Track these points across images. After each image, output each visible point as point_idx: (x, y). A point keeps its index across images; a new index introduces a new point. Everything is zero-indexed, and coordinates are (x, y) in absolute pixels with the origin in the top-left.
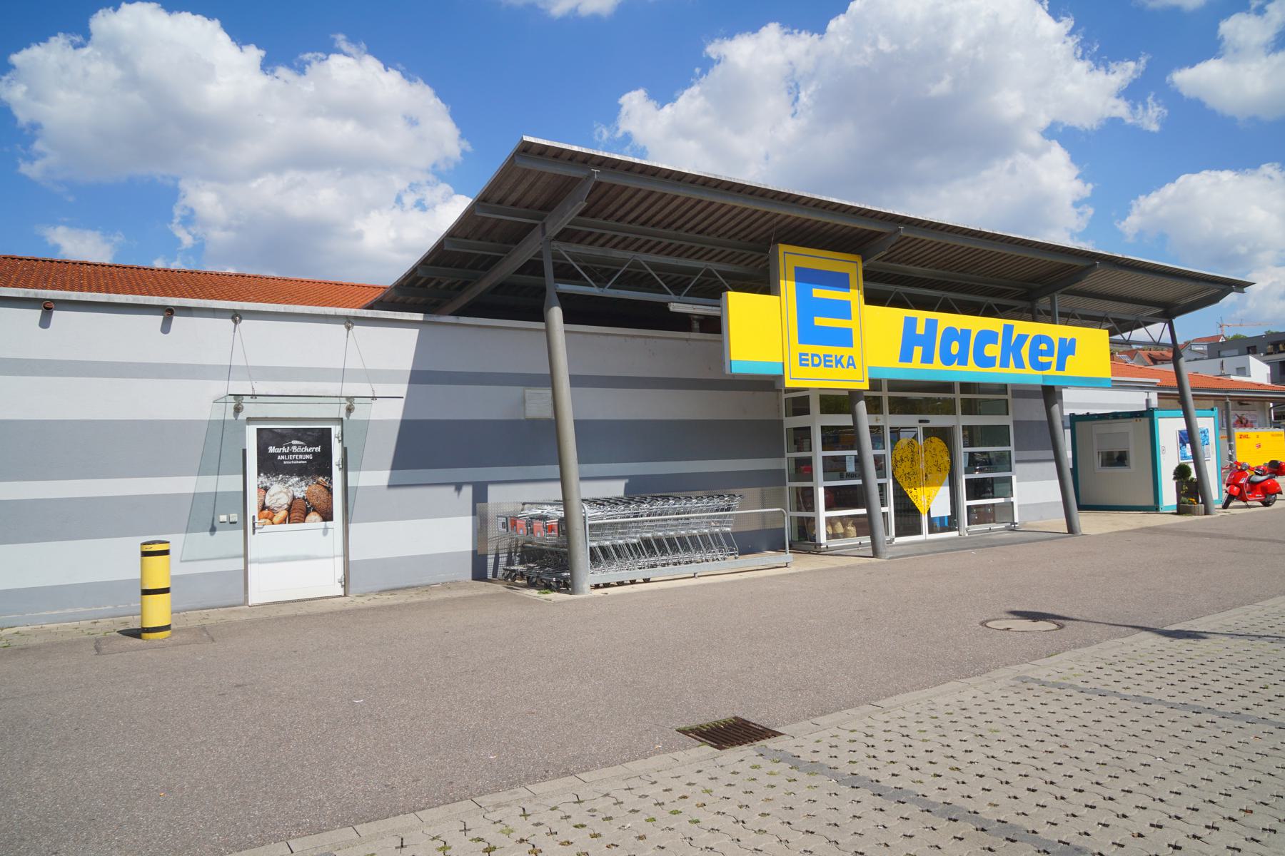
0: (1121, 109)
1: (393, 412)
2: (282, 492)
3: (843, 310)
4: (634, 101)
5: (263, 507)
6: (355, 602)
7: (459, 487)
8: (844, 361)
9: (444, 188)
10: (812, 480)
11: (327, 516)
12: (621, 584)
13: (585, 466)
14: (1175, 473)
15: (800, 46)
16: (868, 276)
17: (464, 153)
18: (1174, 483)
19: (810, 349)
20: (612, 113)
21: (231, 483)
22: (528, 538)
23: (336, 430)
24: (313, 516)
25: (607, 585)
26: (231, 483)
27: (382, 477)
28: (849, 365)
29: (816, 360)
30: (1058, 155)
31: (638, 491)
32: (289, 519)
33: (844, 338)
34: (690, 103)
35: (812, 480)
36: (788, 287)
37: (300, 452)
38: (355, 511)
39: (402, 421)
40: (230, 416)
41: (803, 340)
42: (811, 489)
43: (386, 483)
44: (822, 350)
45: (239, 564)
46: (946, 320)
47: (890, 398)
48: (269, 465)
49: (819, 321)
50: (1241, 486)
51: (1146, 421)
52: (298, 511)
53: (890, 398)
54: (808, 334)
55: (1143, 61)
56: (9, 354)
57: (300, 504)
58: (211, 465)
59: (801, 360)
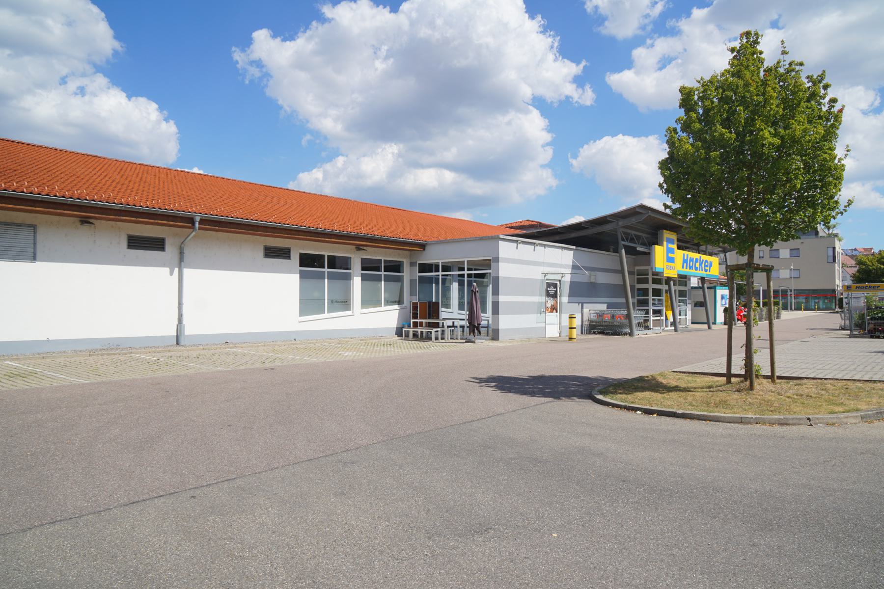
0: (570, 90)
1: (568, 278)
4: (261, 36)
7: (579, 303)
9: (101, 80)
10: (648, 307)
14: (724, 310)
15: (383, 16)
16: (678, 240)
17: (115, 53)
18: (723, 314)
20: (246, 43)
22: (611, 320)
30: (535, 113)
34: (303, 44)
35: (648, 307)
42: (648, 310)
43: (567, 301)
47: (328, 268)
50: (741, 316)
51: (713, 290)
53: (328, 268)
55: (584, 63)
56: (3, 220)
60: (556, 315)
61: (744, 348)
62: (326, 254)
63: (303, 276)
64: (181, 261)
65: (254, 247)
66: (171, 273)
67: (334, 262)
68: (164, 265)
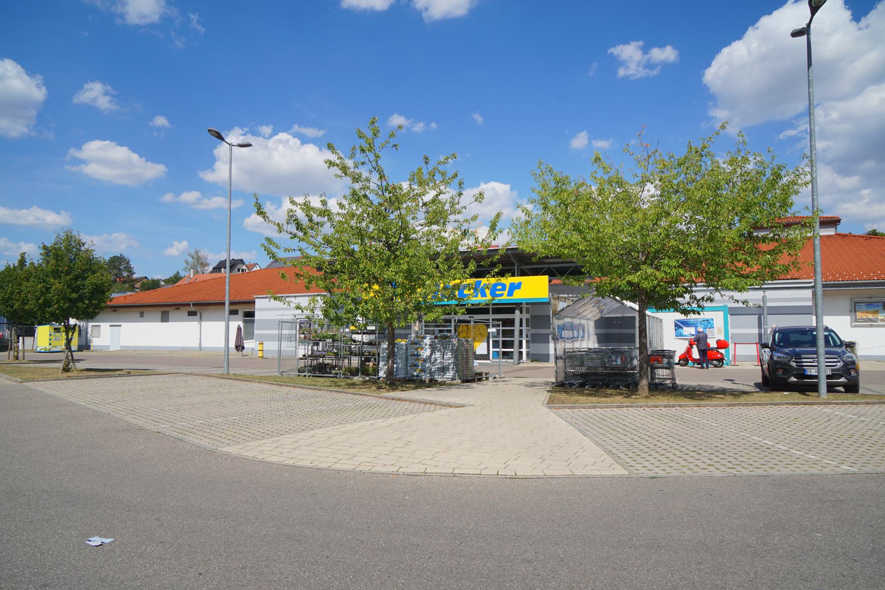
45: (294, 349)
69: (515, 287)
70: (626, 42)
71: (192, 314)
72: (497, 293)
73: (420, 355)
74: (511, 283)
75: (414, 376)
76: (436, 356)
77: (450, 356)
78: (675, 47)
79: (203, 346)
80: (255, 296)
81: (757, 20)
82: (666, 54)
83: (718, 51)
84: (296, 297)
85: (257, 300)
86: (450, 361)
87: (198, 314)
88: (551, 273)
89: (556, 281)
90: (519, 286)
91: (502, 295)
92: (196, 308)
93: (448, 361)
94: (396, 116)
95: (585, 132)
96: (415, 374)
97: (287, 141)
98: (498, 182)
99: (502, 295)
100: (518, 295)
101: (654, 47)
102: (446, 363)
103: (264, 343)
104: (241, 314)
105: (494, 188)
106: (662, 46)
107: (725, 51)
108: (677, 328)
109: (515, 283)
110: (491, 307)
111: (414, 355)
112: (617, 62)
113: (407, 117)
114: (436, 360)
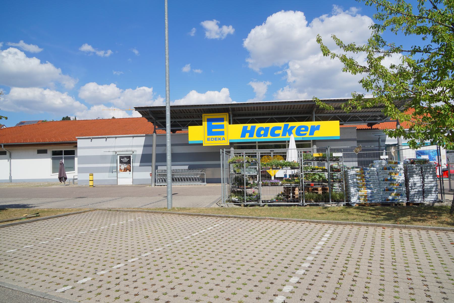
2: (123, 166)
3: (222, 127)
5: (120, 169)
6: (134, 185)
8: (221, 139)
11: (130, 171)
12: (164, 186)
13: (173, 163)
19: (209, 137)
21: (115, 165)
23: (131, 156)
24: (128, 171)
25: (160, 186)
26: (115, 165)
27: (138, 164)
28: (223, 139)
29: (212, 139)
31: (191, 168)
32: (124, 171)
33: (222, 133)
36: (205, 124)
37: (126, 160)
38: (134, 171)
39: (142, 154)
40: (115, 154)
41: (209, 134)
44: (214, 137)
45: (116, 178)
46: (258, 126)
47: (64, 155)
48: (121, 162)
49: (214, 130)
52: (126, 170)
53: (64, 155)
54: (210, 133)
57: (126, 169)
58: (112, 162)
59: (208, 139)
60: (130, 173)
61: (14, 226)
62: (63, 150)
63: (53, 159)
64: (10, 157)
65: (34, 151)
66: (8, 161)
67: (67, 153)
68: (6, 159)
69: (314, 129)
70: (211, 19)
71: (40, 152)
72: (301, 133)
73: (395, 180)
74: (311, 126)
75: (389, 200)
76: (415, 180)
77: (433, 180)
78: (233, 27)
79: (13, 179)
80: (77, 137)
81: (265, 19)
82: (228, 30)
83: (249, 31)
84: (116, 137)
85: (78, 141)
86: (433, 185)
87: (8, 154)
88: (343, 119)
89: (346, 125)
90: (318, 128)
91: (305, 134)
92: (6, 148)
93: (430, 185)
94: (86, 45)
95: (189, 65)
96: (390, 198)
97: (16, 53)
98: (146, 87)
99: (305, 134)
100: (317, 135)
101: (223, 25)
102: (427, 186)
103: (94, 174)
104: (50, 152)
105: (144, 90)
106: (228, 25)
107: (253, 31)
108: (417, 156)
109: (315, 126)
110: (257, 144)
111: (387, 180)
112: (202, 30)
113: (94, 47)
114: (415, 184)
